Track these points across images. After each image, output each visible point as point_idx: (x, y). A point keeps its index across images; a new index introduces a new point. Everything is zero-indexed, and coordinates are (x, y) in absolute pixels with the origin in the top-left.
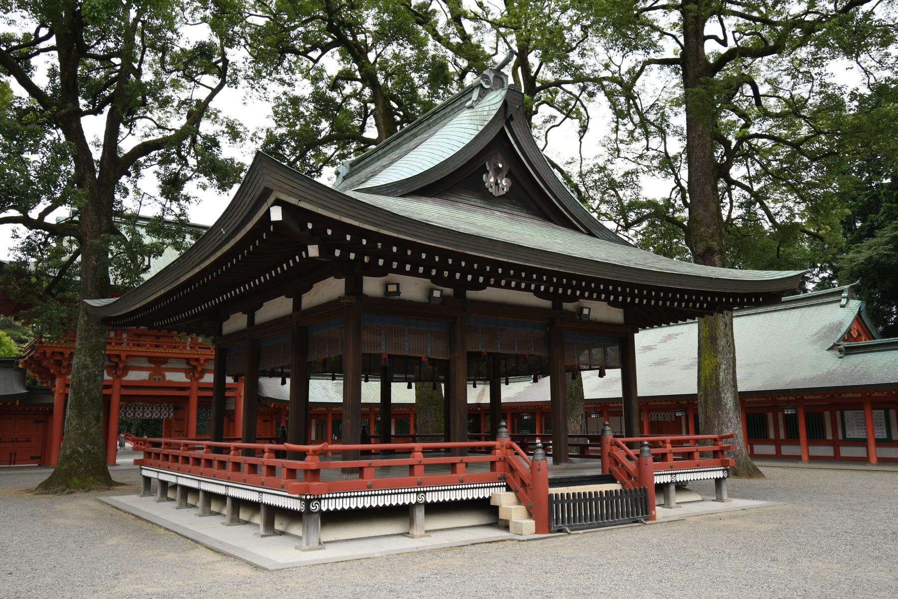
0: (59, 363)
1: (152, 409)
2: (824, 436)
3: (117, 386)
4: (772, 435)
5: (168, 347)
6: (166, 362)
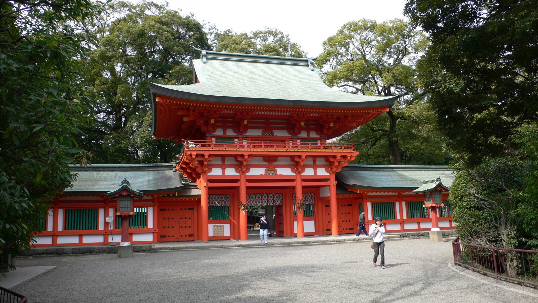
0: (201, 163)
1: (221, 198)
2: (395, 217)
3: (243, 181)
4: (398, 217)
5: (278, 147)
6: (276, 161)
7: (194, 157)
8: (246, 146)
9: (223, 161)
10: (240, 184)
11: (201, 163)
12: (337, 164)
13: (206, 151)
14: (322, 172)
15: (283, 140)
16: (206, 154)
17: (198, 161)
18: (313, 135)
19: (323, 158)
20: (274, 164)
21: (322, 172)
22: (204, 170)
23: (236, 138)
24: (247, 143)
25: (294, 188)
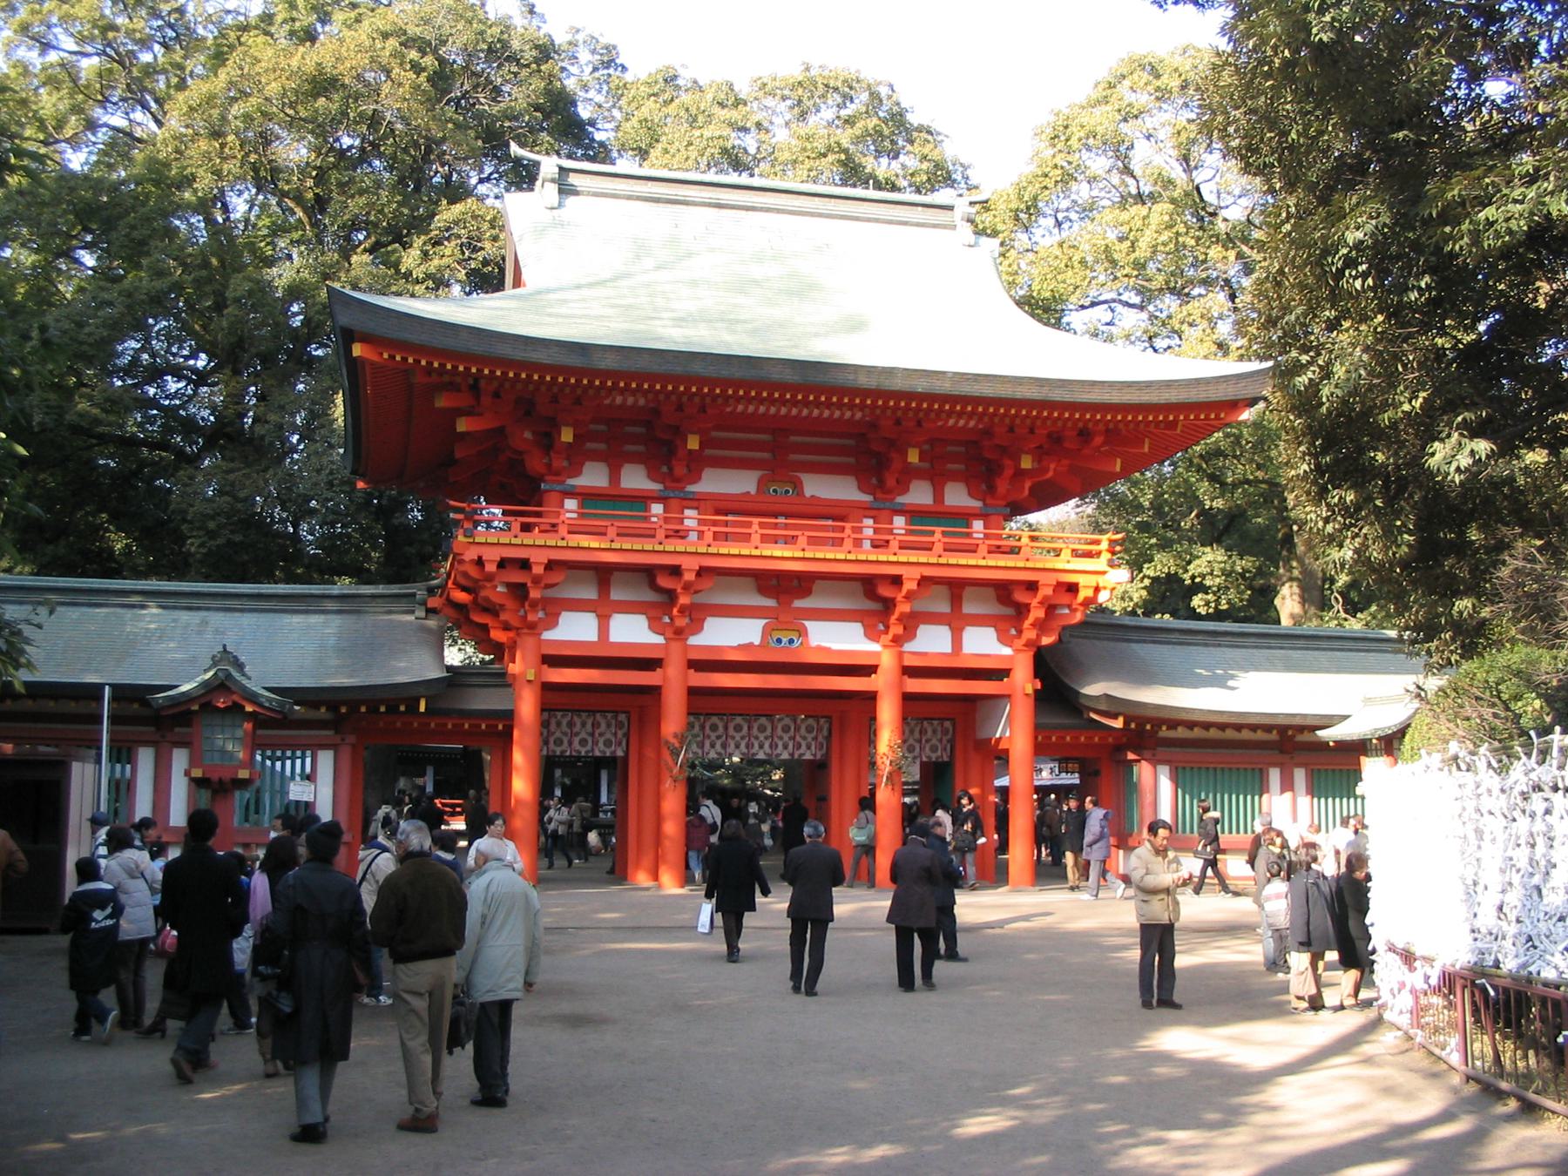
0: (519, 592)
6: (806, 592)
7: (491, 568)
8: (693, 536)
9: (956, 601)
10: (686, 677)
11: (519, 592)
12: (1037, 613)
13: (538, 546)
14: (982, 643)
15: (839, 513)
16: (539, 558)
17: (508, 585)
18: (957, 496)
19: (591, 573)
20: (798, 603)
21: (982, 643)
22: (531, 618)
23: (978, 516)
24: (701, 522)
25: (654, 692)
